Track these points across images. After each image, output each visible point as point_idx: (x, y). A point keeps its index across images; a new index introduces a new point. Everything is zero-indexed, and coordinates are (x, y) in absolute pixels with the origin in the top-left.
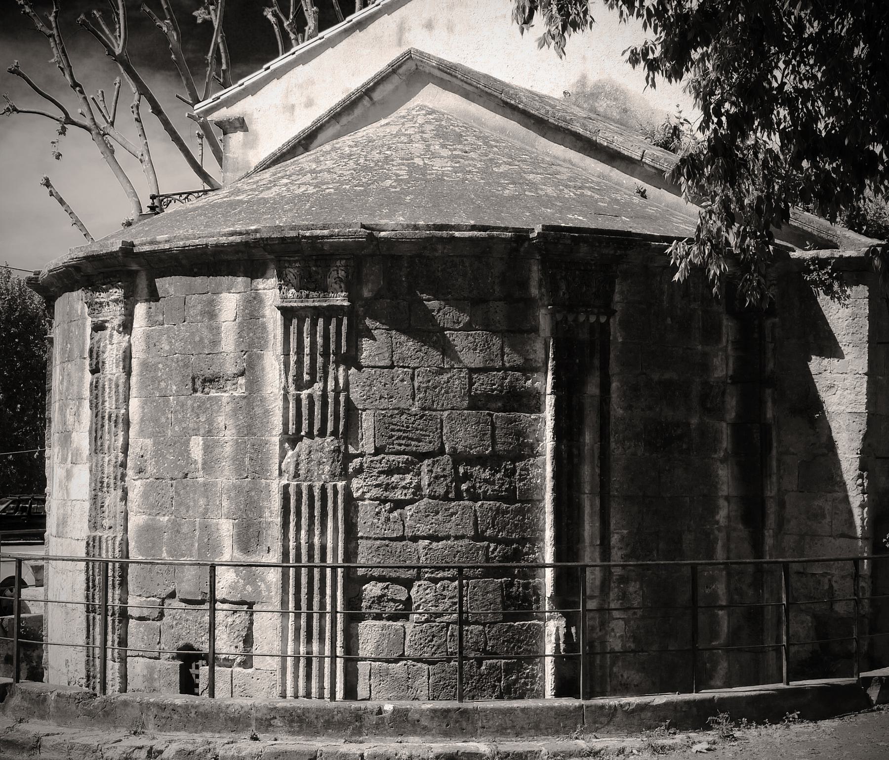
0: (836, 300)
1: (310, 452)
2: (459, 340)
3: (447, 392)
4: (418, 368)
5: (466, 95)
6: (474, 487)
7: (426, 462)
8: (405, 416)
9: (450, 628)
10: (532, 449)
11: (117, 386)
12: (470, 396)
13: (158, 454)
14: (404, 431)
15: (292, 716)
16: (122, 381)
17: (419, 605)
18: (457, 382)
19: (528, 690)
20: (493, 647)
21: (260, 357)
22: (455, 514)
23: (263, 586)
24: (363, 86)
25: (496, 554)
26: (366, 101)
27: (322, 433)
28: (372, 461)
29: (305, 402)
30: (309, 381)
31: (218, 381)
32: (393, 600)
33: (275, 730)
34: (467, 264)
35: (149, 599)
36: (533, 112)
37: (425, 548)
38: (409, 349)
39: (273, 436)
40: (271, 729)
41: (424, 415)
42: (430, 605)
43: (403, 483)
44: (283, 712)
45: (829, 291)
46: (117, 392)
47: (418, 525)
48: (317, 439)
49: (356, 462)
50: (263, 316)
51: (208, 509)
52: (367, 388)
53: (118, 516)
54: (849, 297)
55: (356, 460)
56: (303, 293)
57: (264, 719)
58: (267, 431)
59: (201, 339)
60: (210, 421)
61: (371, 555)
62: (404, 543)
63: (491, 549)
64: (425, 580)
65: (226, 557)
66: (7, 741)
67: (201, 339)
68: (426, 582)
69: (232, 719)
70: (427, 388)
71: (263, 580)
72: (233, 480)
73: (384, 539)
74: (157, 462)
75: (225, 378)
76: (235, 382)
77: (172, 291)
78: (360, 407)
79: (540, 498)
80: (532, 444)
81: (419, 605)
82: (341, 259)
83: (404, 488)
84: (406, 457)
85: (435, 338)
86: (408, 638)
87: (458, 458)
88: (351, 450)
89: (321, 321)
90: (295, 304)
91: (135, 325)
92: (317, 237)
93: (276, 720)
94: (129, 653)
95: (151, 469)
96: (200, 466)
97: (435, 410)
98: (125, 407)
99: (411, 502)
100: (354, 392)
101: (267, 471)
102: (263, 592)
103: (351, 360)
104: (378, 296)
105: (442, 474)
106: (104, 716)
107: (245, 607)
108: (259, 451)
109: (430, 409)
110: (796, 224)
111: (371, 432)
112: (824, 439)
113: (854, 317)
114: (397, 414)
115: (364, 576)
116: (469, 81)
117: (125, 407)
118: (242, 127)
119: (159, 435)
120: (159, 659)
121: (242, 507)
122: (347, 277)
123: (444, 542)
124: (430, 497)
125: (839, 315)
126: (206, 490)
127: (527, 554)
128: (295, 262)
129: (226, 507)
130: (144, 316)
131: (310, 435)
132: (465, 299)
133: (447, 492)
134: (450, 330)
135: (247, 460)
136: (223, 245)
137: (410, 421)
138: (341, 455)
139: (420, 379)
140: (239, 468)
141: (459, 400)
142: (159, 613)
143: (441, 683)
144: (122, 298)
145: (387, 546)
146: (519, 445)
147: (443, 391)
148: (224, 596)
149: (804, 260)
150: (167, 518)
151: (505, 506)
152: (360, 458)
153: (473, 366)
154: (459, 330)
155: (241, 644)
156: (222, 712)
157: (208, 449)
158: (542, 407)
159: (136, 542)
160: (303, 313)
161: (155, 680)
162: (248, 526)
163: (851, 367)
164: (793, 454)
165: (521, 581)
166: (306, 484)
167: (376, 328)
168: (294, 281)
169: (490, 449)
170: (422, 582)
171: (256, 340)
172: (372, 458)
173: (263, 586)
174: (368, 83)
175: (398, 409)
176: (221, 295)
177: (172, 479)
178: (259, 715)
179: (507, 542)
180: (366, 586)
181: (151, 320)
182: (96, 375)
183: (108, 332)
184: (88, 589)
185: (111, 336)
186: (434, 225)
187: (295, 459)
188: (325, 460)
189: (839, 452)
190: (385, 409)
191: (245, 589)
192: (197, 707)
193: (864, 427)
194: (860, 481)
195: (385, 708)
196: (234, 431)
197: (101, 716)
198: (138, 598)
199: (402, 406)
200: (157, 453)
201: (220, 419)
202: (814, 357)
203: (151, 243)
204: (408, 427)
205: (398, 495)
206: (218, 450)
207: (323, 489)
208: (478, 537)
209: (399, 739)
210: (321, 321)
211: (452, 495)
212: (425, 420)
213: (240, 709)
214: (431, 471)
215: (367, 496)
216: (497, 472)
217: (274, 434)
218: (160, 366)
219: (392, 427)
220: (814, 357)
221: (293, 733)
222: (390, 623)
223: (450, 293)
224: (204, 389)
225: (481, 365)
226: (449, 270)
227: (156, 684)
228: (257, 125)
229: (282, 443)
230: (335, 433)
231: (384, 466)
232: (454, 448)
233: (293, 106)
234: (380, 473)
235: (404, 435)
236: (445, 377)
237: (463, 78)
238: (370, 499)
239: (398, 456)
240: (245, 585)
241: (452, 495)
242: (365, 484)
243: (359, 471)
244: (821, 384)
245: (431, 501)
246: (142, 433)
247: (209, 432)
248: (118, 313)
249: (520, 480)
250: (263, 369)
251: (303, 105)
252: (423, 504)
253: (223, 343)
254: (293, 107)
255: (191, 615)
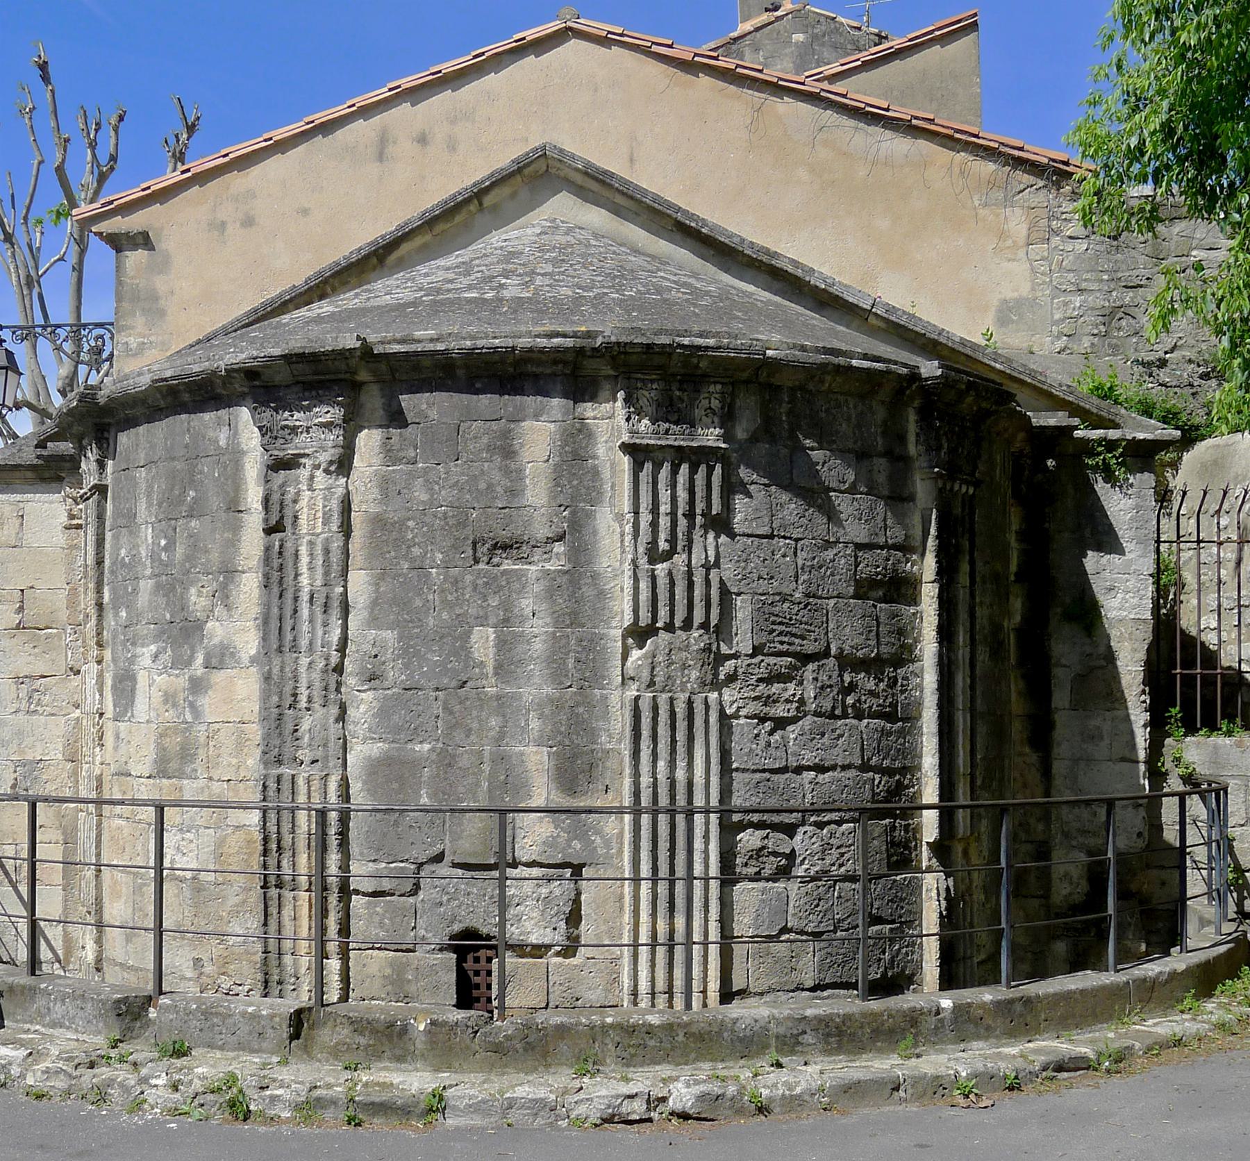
0: (1117, 489)
1: (670, 651)
2: (844, 505)
3: (832, 574)
4: (801, 539)
5: (616, 211)
6: (859, 701)
7: (810, 667)
8: (786, 605)
9: (837, 888)
10: (911, 652)
11: (327, 551)
12: (856, 580)
13: (408, 653)
14: (787, 625)
15: (828, 1027)
16: (337, 544)
17: (805, 858)
18: (843, 562)
19: (908, 961)
20: (878, 909)
21: (590, 515)
22: (842, 736)
23: (598, 841)
24: (474, 185)
25: (881, 788)
26: (473, 207)
27: (687, 625)
28: (749, 665)
29: (662, 582)
30: (667, 551)
31: (518, 548)
32: (775, 854)
33: (805, 1049)
34: (851, 406)
35: (392, 865)
36: (723, 240)
37: (811, 783)
38: (791, 513)
39: (611, 628)
40: (799, 1048)
41: (808, 604)
42: (816, 858)
43: (786, 695)
44: (815, 1022)
45: (1110, 478)
46: (326, 562)
47: (803, 752)
48: (679, 632)
49: (729, 665)
50: (595, 457)
51: (505, 733)
52: (743, 564)
53: (331, 745)
54: (1131, 485)
55: (728, 663)
56: (661, 427)
57: (789, 1035)
58: (602, 621)
59: (490, 487)
60: (507, 606)
61: (749, 793)
62: (787, 775)
63: (876, 782)
64: (810, 825)
65: (538, 801)
66: (373, 1104)
67: (490, 487)
68: (811, 828)
69: (741, 1040)
70: (812, 566)
71: (598, 832)
72: (548, 690)
73: (764, 771)
74: (407, 666)
75: (531, 543)
76: (548, 549)
77: (433, 414)
78: (734, 590)
79: (917, 716)
80: (911, 645)
81: (805, 858)
82: (715, 383)
83: (787, 701)
84: (789, 659)
85: (820, 501)
86: (791, 905)
87: (847, 662)
88: (724, 649)
89: (684, 469)
90: (653, 442)
91: (356, 463)
92: (699, 348)
93: (806, 1036)
94: (351, 946)
95: (394, 674)
96: (490, 670)
97: (820, 598)
98: (342, 583)
99: (794, 720)
100: (725, 570)
101: (604, 678)
102: (599, 849)
103: (721, 524)
104: (754, 439)
105: (828, 683)
106: (525, 1050)
107: (568, 873)
108: (591, 649)
109: (814, 596)
110: (1071, 399)
111: (748, 625)
112: (1102, 649)
113: (1138, 508)
114: (779, 601)
115: (741, 822)
116: (630, 193)
117: (342, 583)
118: (146, 244)
119: (411, 625)
120: (415, 951)
121: (563, 729)
122: (722, 408)
123: (830, 773)
124: (817, 714)
125: (1121, 506)
126: (501, 706)
127: (908, 787)
128: (652, 381)
129: (537, 729)
130: (377, 450)
131: (669, 627)
132: (849, 451)
133: (834, 708)
134: (835, 491)
135: (571, 663)
136: (542, 351)
137: (794, 612)
138: (712, 656)
139: (804, 554)
140: (557, 674)
141: (844, 585)
142: (414, 884)
143: (828, 961)
144: (340, 422)
145: (768, 780)
146: (901, 646)
147: (828, 573)
148: (534, 857)
149: (1089, 441)
150: (427, 747)
151: (888, 726)
152: (734, 661)
153: (858, 540)
154: (842, 492)
155: (563, 925)
156: (726, 1030)
157: (503, 645)
158: (918, 599)
159: (365, 783)
160: (659, 455)
161: (409, 981)
162: (574, 757)
163: (1134, 567)
164: (1065, 666)
165: (903, 823)
166: (665, 696)
167: (753, 483)
168: (649, 409)
169: (876, 650)
170: (807, 828)
171: (583, 491)
172: (749, 662)
173: (598, 841)
174: (483, 182)
175: (779, 594)
176: (523, 424)
177: (437, 689)
178: (781, 1030)
179: (889, 772)
180: (741, 835)
181: (389, 454)
182: (277, 536)
183: (304, 473)
184: (265, 853)
185: (312, 478)
186: (824, 348)
187: (650, 661)
188: (692, 663)
189: (1119, 663)
190: (764, 594)
191: (570, 846)
192: (687, 1025)
193: (1149, 636)
194: (1143, 698)
195: (943, 1006)
196: (548, 620)
197: (521, 1051)
198: (371, 864)
199: (786, 591)
200: (406, 651)
201: (524, 603)
202: (1090, 553)
203: (402, 341)
204: (791, 619)
205: (780, 711)
206: (520, 648)
207: (690, 703)
208: (865, 767)
209: (962, 1046)
210: (684, 469)
211: (838, 712)
212: (810, 610)
213: (753, 1024)
214: (816, 679)
215: (743, 712)
216: (881, 680)
217: (614, 625)
218: (411, 523)
219: (772, 618)
220: (1090, 553)
221: (828, 1052)
222: (770, 884)
223: (834, 442)
224: (491, 559)
225: (866, 541)
226: (834, 411)
227: (412, 989)
228: (167, 242)
229: (624, 638)
230: (705, 626)
231: (762, 672)
232: (841, 648)
233: (223, 224)
234: (760, 680)
235: (787, 629)
236: (830, 553)
237: (621, 188)
238: (746, 717)
239: (779, 659)
240: (569, 841)
241: (838, 712)
242: (740, 696)
243: (732, 678)
244: (1098, 586)
245: (816, 719)
246: (373, 621)
247: (506, 621)
248: (330, 444)
249: (902, 692)
250: (595, 533)
251: (238, 224)
252: (808, 723)
253: (528, 493)
254: (223, 225)
255: (474, 885)
